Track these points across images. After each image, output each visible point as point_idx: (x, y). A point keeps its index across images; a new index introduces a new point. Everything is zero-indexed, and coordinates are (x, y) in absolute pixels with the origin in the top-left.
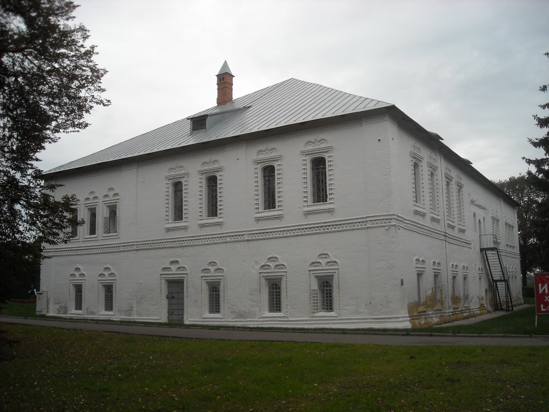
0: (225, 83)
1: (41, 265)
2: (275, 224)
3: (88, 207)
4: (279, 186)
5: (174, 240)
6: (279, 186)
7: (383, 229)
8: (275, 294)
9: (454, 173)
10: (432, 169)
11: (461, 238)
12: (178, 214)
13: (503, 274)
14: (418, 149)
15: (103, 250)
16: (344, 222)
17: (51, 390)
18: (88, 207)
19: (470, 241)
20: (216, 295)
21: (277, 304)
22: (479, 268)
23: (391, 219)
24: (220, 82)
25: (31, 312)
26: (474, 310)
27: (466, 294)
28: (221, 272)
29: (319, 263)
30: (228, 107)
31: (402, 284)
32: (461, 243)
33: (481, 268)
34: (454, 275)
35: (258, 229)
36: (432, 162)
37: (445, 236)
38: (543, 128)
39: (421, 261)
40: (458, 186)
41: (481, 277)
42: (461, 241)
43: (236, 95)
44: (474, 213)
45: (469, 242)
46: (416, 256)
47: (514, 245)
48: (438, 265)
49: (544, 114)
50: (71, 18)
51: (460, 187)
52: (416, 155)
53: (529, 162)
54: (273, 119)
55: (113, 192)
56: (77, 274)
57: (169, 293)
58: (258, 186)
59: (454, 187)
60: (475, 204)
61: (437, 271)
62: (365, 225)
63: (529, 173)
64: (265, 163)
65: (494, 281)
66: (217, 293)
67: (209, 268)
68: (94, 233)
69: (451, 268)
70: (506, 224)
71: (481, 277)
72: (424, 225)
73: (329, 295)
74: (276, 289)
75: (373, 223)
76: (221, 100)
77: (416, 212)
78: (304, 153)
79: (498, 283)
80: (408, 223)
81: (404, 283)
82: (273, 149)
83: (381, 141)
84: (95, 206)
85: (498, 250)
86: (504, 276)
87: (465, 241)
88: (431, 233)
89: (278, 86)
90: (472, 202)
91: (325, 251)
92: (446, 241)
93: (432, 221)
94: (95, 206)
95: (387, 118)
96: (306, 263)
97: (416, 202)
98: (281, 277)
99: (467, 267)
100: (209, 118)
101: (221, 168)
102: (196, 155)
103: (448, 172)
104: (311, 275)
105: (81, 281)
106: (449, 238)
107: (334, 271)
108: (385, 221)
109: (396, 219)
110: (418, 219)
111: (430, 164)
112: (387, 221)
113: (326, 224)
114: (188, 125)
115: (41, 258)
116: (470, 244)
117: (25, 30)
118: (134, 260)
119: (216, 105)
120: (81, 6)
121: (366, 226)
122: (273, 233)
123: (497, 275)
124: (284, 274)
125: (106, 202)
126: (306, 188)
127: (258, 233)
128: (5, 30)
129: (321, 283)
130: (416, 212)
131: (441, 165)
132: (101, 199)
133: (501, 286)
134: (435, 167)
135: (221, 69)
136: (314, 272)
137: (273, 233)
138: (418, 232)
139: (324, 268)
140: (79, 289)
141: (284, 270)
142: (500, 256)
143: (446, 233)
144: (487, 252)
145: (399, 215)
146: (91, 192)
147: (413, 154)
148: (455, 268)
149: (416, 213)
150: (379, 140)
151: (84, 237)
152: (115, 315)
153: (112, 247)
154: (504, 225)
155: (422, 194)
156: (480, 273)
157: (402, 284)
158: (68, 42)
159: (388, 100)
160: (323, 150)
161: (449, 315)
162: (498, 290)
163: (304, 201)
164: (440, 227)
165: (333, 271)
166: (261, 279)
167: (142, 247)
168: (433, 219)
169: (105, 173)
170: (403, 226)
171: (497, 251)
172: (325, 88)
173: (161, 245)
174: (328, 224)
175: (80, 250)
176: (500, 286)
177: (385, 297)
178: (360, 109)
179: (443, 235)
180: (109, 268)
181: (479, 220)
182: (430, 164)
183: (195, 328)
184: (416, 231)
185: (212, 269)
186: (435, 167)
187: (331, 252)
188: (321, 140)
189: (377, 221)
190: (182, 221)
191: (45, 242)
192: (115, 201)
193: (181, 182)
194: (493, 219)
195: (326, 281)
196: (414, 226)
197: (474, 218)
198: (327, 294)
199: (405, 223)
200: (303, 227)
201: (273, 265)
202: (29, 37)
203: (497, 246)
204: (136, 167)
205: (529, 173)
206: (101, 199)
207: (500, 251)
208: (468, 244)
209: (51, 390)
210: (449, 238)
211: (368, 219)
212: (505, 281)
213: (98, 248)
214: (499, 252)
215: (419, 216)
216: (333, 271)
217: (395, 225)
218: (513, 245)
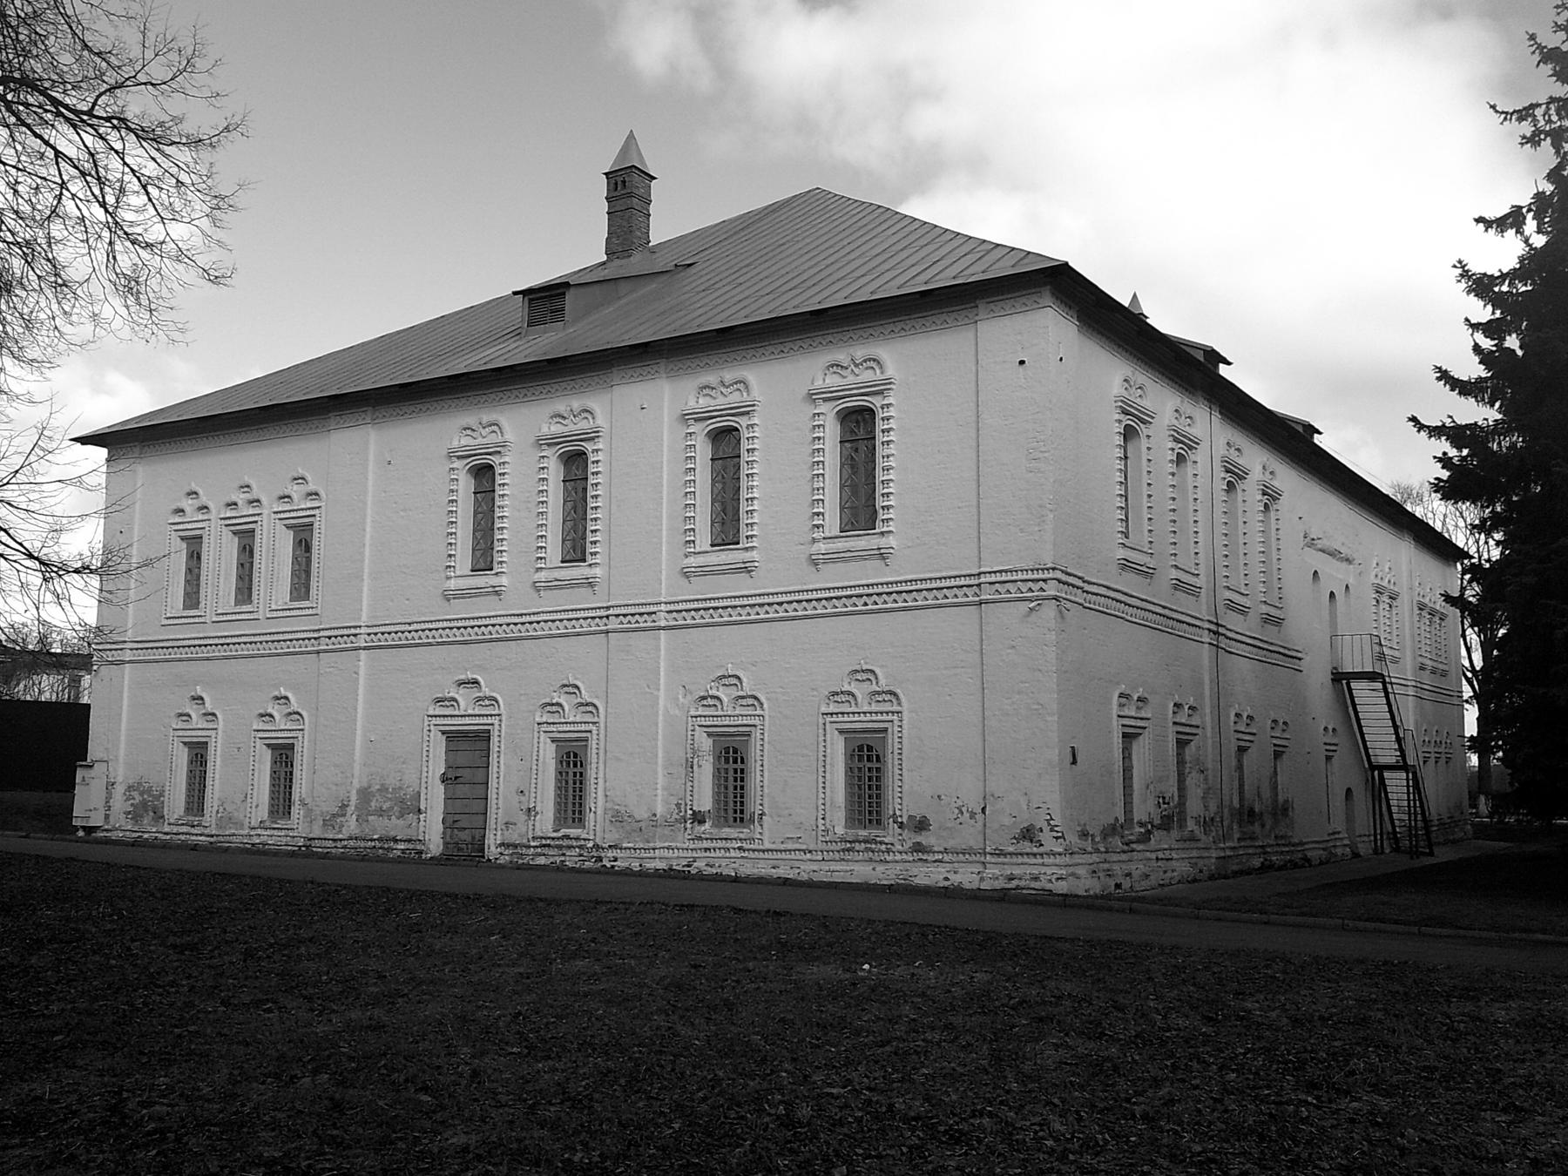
0: (630, 195)
1: (1483, 303)
2: (581, 599)
3: (267, 742)
4: (750, 483)
5: (476, 623)
6: (750, 483)
7: (1024, 607)
8: (731, 772)
9: (1257, 459)
10: (1180, 445)
11: (1270, 641)
12: (484, 560)
13: (1401, 750)
14: (1140, 388)
15: (278, 647)
16: (919, 586)
17: (1502, 615)
18: (233, 528)
19: (1297, 651)
20: (735, 771)
21: (574, 796)
22: (1326, 729)
23: (1045, 580)
24: (617, 194)
25: (59, 818)
26: (1306, 846)
27: (1281, 799)
28: (591, 712)
29: (850, 693)
30: (636, 263)
31: (1074, 762)
32: (1268, 654)
33: (1334, 730)
34: (1243, 744)
35: (692, 597)
36: (1182, 424)
37: (1214, 633)
38: (1433, 439)
39: (1136, 698)
40: (1264, 494)
41: (1331, 754)
42: (1267, 650)
43: (660, 232)
44: (1316, 572)
45: (1294, 654)
46: (1118, 683)
47: (1445, 667)
48: (1249, 721)
49: (1553, 40)
50: (1167, 622)
51: (1271, 496)
52: (1130, 406)
53: (1475, 327)
54: (550, 612)
55: (197, 503)
56: (296, 491)
57: (448, 767)
58: (694, 481)
59: (1250, 492)
60: (1319, 546)
61: (1187, 730)
62: (1042, 589)
63: (1533, 219)
64: (714, 420)
65: (1373, 767)
66: (739, 766)
67: (853, 688)
68: (196, 605)
69: (1232, 724)
70: (1422, 607)
71: (1331, 754)
72: (1149, 599)
73: (874, 782)
74: (869, 760)
75: (965, 594)
76: (95, 149)
77: (1125, 562)
78: (452, 455)
79: (1386, 774)
80: (1097, 594)
81: (1079, 759)
82: (736, 383)
83: (1021, 369)
84: (251, 526)
85: (1387, 679)
86: (1403, 755)
87: (1282, 650)
88: (1171, 623)
89: (774, 211)
90: (1311, 543)
91: (866, 663)
92: (1217, 646)
93: (1176, 589)
94: (251, 526)
95: (1047, 299)
96: (815, 693)
97: (1127, 537)
98: (584, 735)
99: (1285, 723)
100: (570, 296)
101: (598, 432)
102: (311, 428)
103: (1233, 454)
104: (828, 725)
105: (485, 720)
106: (1227, 638)
107: (890, 717)
108: (1030, 584)
109: (1060, 581)
110: (1129, 583)
111: (1174, 430)
112: (1035, 587)
113: (871, 591)
114: (520, 309)
115: (1533, 207)
116: (1300, 659)
117: (1484, 374)
118: (948, 698)
119: (605, 258)
120: (222, 503)
121: (977, 599)
122: (711, 611)
123: (1384, 749)
124: (756, 721)
125: (282, 516)
126: (821, 491)
127: (709, 609)
128: (1489, 686)
129: (854, 751)
130: (1125, 562)
131: (1207, 425)
132: (270, 505)
133: (1396, 783)
134: (1190, 440)
135: (1238, 388)
136: (835, 718)
137: (711, 611)
138: (1129, 618)
139: (864, 711)
140: (198, 754)
141: (757, 712)
142: (1391, 696)
143: (1217, 624)
144: (1385, 774)
145: (1069, 570)
146: (311, 494)
147: (1122, 401)
148: (1248, 725)
149: (1126, 565)
150: (1022, 362)
151: (219, 612)
152: (300, 827)
153: (297, 640)
154: (1416, 609)
155: (1146, 479)
156: (1328, 741)
157: (1074, 762)
158: (135, 1122)
159: (1057, 250)
160: (868, 387)
161: (1224, 857)
162: (1386, 793)
163: (814, 525)
164: (1159, 592)
165: (885, 717)
166: (696, 733)
167: (393, 640)
168: (1179, 585)
169: (218, 444)
170: (1081, 601)
171: (1384, 683)
172: (995, 251)
173: (434, 637)
174: (876, 590)
175: (206, 646)
176: (1395, 797)
177: (1026, 794)
178: (976, 274)
179: (1210, 630)
180: (286, 698)
181: (1332, 595)
182: (1174, 430)
183: (1445, 931)
184: (1124, 615)
185: (860, 691)
186: (1190, 440)
187: (882, 666)
188: (865, 361)
189: (1009, 586)
190: (493, 572)
191: (1447, 440)
192: (308, 513)
193: (585, 454)
194: (1377, 592)
195: (868, 746)
196: (1117, 601)
197: (1346, 596)
198: (870, 779)
199: (1088, 592)
200: (810, 596)
201: (726, 695)
202: (1520, 353)
203: (1384, 667)
204: (137, 450)
205: (1533, 219)
206: (270, 505)
207: (1391, 683)
208: (1290, 659)
209: (1502, 615)
210: (1227, 638)
211: (322, 633)
212: (1404, 767)
213: (256, 643)
214: (1389, 686)
215: (1134, 575)
216: (885, 717)
217: (1056, 598)
218: (1440, 666)
